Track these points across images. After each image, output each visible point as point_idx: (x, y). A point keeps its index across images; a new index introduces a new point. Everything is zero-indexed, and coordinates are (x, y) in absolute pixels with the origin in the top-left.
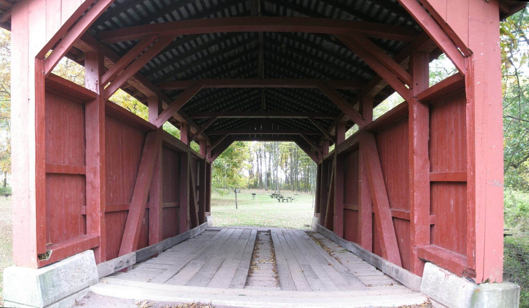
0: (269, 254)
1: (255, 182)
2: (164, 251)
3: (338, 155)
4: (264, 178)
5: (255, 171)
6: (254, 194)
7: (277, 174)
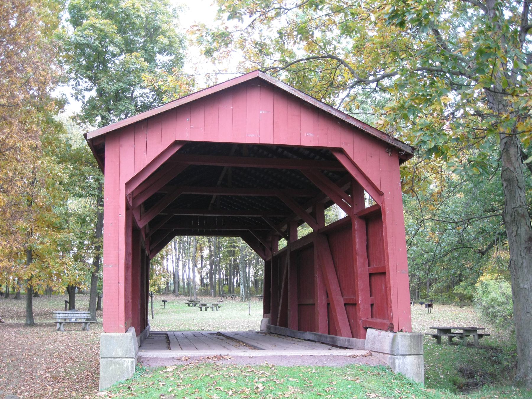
6: (164, 302)
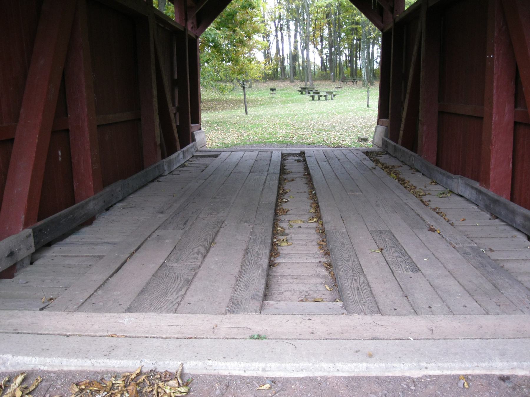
0: (306, 204)
1: (274, 69)
2: (107, 210)
4: (287, 62)
5: (273, 52)
6: (273, 90)
7: (308, 55)
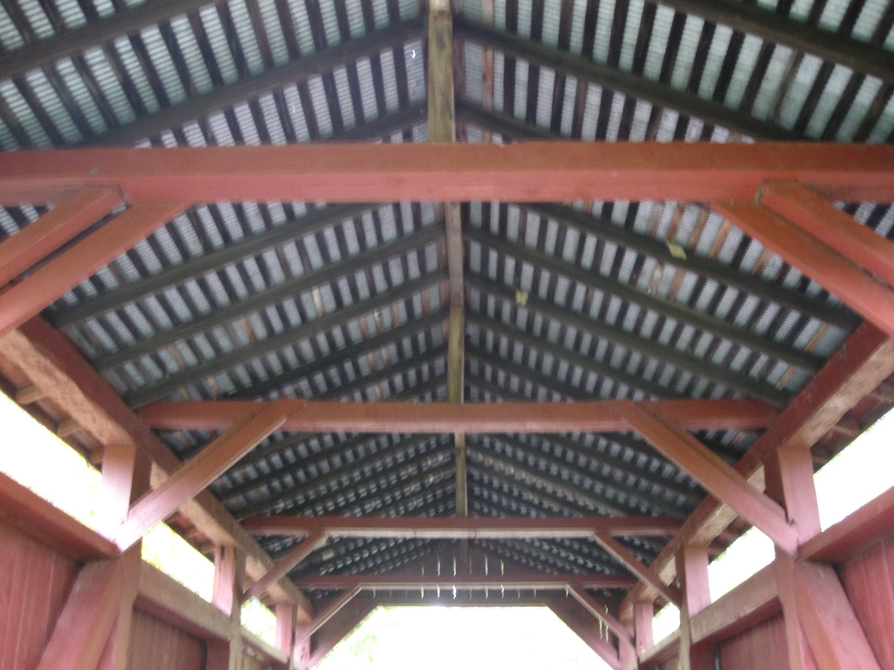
3: (697, 650)
